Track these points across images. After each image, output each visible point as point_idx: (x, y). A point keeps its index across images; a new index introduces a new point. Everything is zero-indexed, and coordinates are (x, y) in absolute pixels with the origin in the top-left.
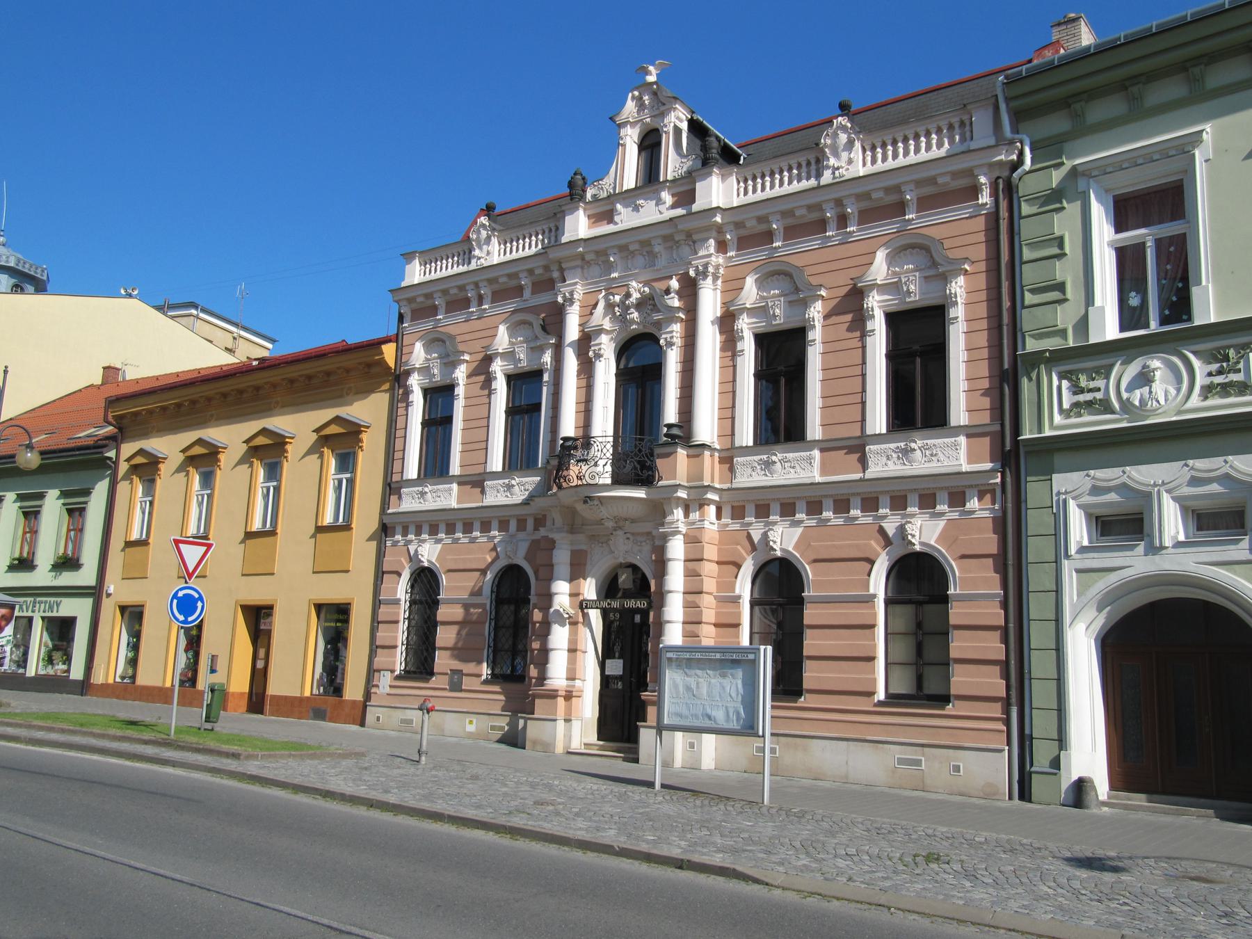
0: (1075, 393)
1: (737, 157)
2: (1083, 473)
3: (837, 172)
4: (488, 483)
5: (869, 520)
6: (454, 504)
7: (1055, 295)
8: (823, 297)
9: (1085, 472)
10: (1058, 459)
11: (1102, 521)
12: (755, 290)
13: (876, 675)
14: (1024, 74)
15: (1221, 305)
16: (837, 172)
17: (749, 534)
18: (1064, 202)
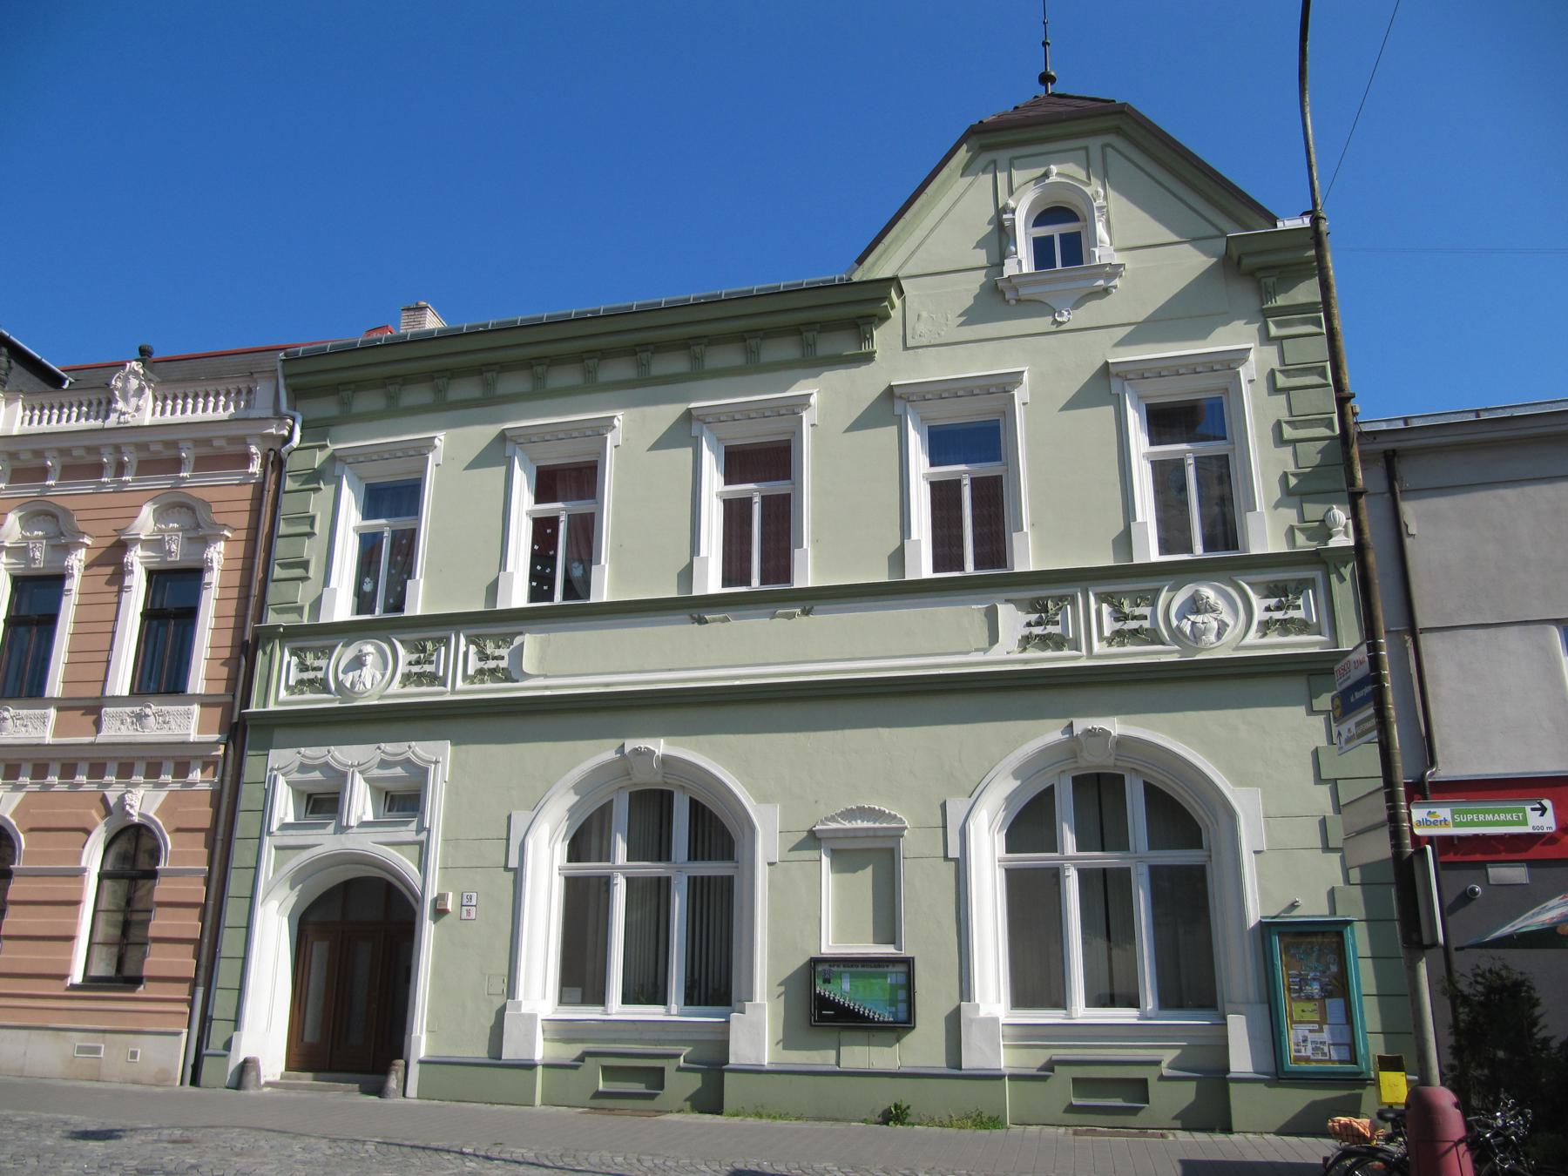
0: (301, 671)
1: (61, 381)
2: (295, 750)
3: (122, 417)
4: (107, 710)
5: (94, 787)
6: (49, 739)
7: (299, 572)
8: (88, 545)
9: (376, 745)
10: (278, 734)
11: (315, 800)
12: (151, 522)
13: (73, 957)
14: (408, 339)
15: (614, 587)
16: (122, 417)
17: (104, 796)
18: (322, 483)
